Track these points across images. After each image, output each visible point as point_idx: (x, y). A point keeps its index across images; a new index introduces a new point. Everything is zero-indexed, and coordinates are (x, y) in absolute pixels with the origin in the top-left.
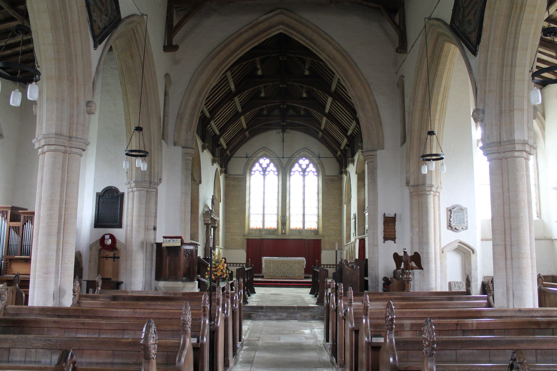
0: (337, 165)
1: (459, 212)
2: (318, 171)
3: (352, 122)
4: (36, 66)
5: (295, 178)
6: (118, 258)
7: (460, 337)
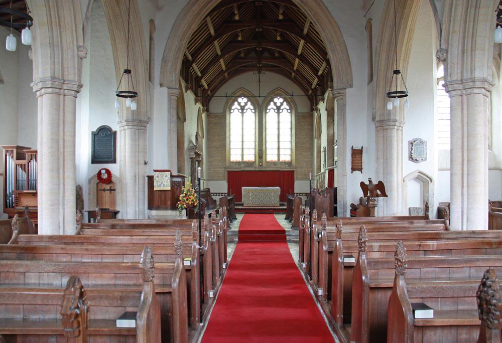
0: (308, 102)
1: (419, 145)
2: (291, 109)
3: (322, 63)
4: (28, 11)
5: (271, 116)
6: (114, 190)
7: (422, 257)
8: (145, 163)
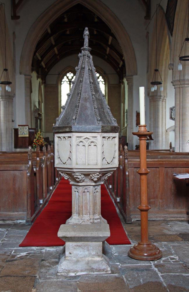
8: (13, 121)
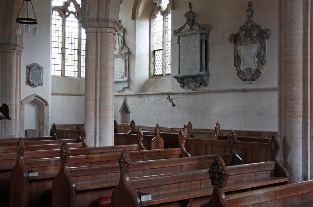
1: (36, 70)
